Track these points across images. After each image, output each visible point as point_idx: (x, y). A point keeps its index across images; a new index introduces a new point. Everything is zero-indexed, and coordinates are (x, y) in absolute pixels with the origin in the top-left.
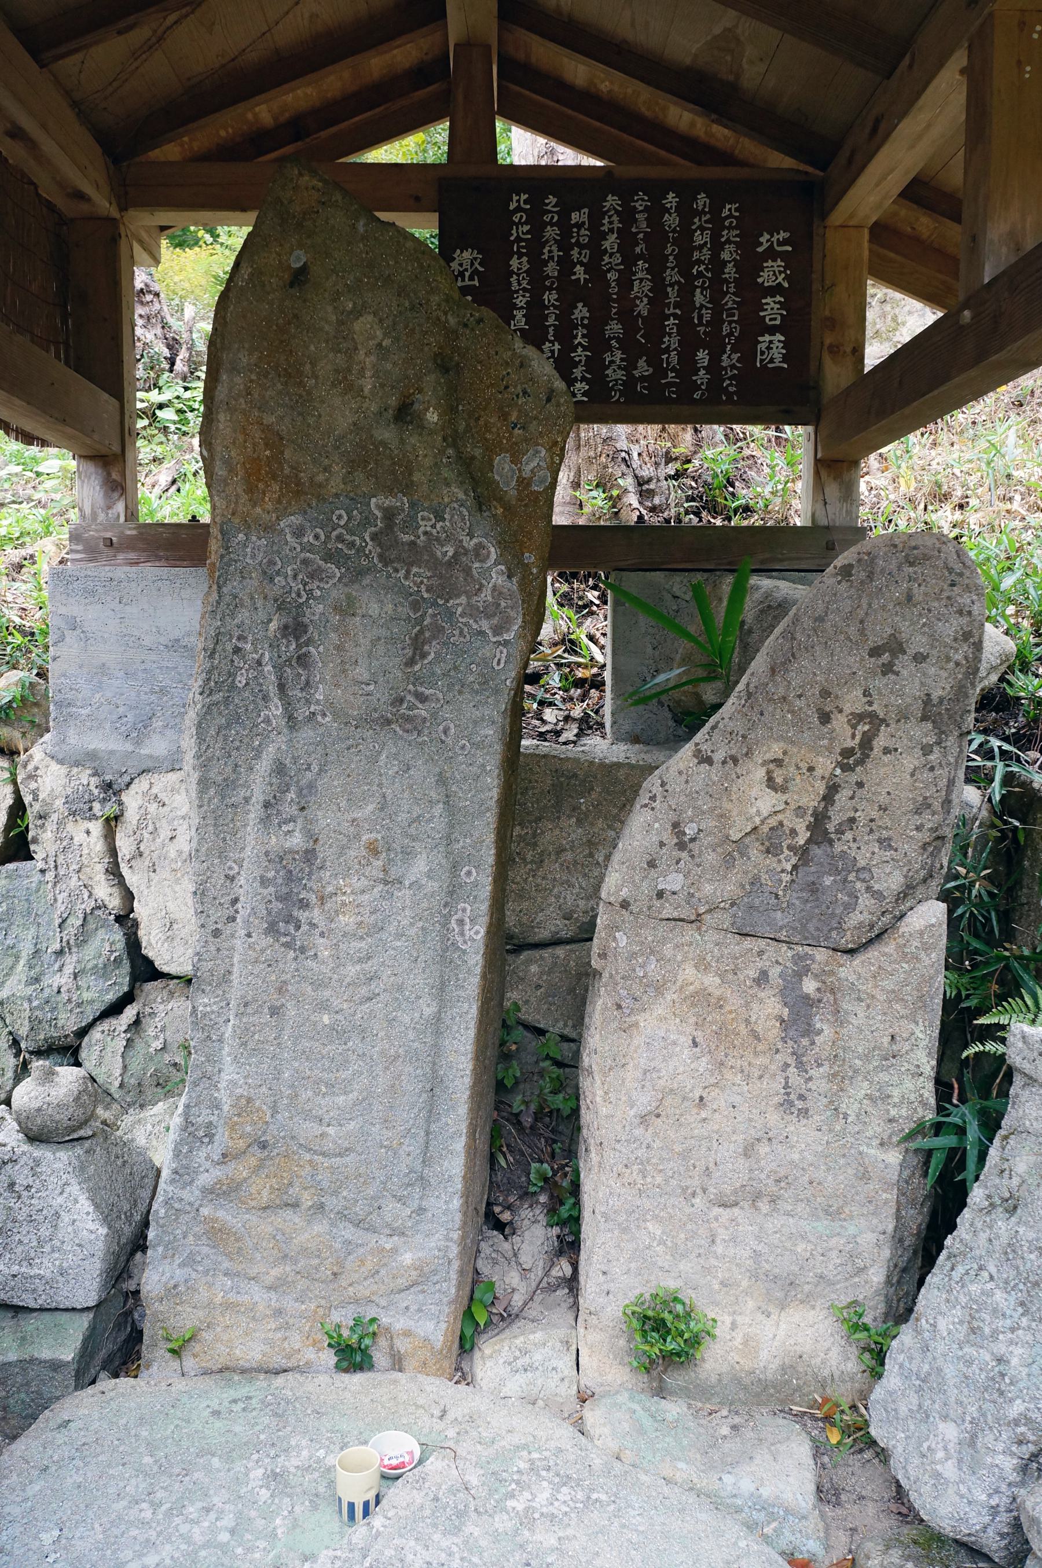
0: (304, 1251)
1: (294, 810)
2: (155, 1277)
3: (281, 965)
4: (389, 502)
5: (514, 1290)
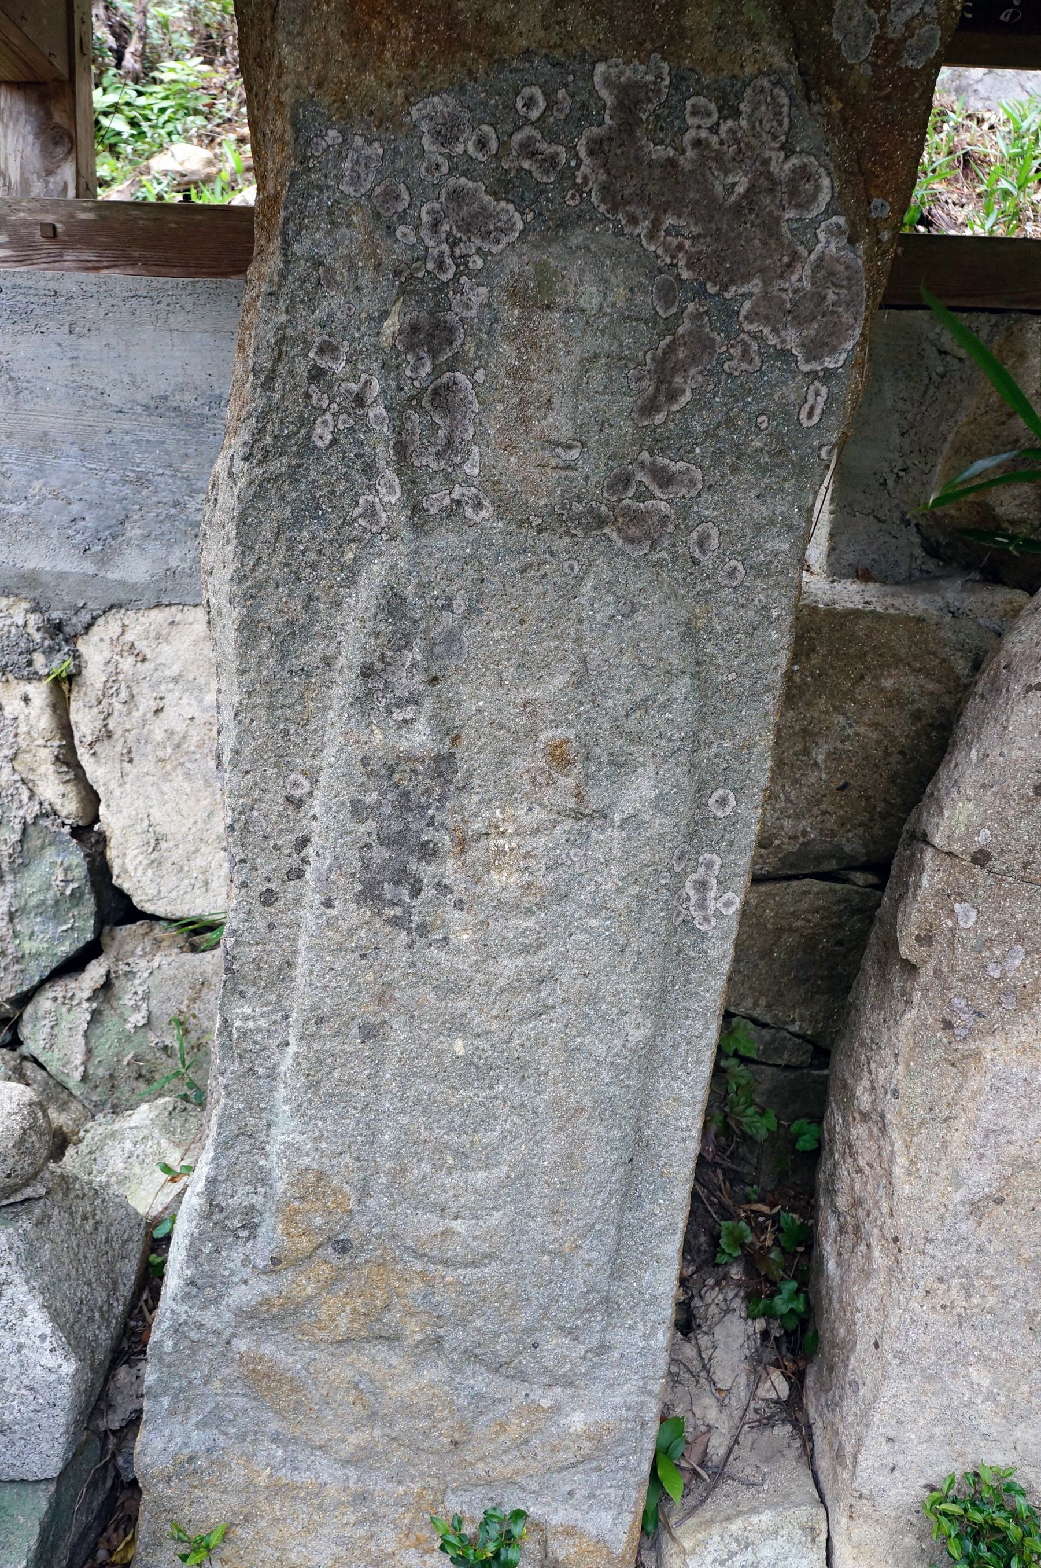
0: (406, 1408)
1: (417, 683)
2: (158, 1444)
3: (383, 956)
4: (634, 72)
5: (710, 1428)
